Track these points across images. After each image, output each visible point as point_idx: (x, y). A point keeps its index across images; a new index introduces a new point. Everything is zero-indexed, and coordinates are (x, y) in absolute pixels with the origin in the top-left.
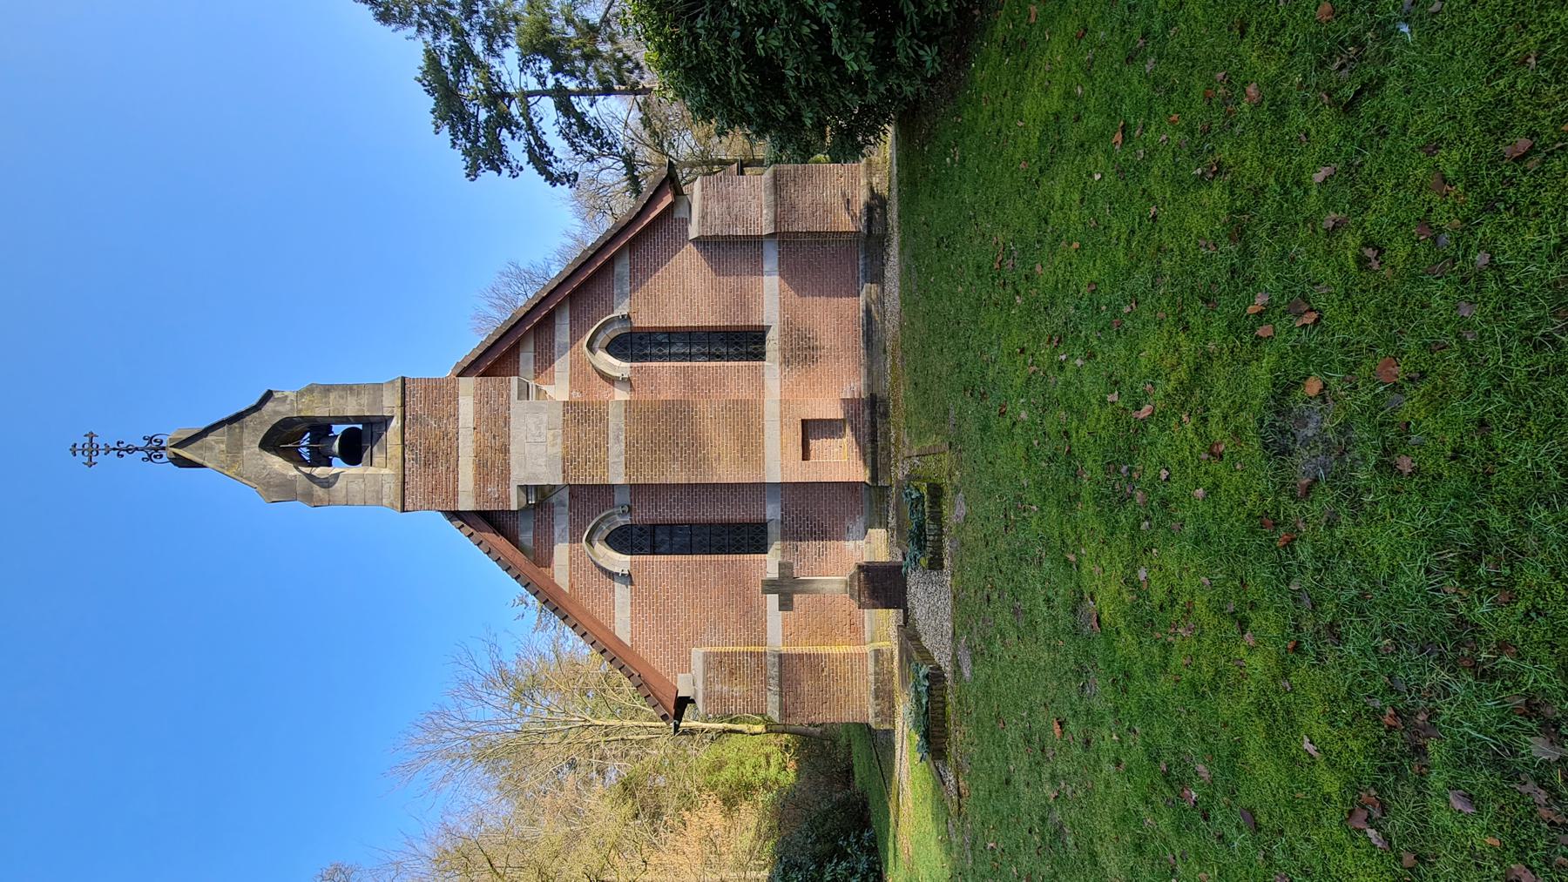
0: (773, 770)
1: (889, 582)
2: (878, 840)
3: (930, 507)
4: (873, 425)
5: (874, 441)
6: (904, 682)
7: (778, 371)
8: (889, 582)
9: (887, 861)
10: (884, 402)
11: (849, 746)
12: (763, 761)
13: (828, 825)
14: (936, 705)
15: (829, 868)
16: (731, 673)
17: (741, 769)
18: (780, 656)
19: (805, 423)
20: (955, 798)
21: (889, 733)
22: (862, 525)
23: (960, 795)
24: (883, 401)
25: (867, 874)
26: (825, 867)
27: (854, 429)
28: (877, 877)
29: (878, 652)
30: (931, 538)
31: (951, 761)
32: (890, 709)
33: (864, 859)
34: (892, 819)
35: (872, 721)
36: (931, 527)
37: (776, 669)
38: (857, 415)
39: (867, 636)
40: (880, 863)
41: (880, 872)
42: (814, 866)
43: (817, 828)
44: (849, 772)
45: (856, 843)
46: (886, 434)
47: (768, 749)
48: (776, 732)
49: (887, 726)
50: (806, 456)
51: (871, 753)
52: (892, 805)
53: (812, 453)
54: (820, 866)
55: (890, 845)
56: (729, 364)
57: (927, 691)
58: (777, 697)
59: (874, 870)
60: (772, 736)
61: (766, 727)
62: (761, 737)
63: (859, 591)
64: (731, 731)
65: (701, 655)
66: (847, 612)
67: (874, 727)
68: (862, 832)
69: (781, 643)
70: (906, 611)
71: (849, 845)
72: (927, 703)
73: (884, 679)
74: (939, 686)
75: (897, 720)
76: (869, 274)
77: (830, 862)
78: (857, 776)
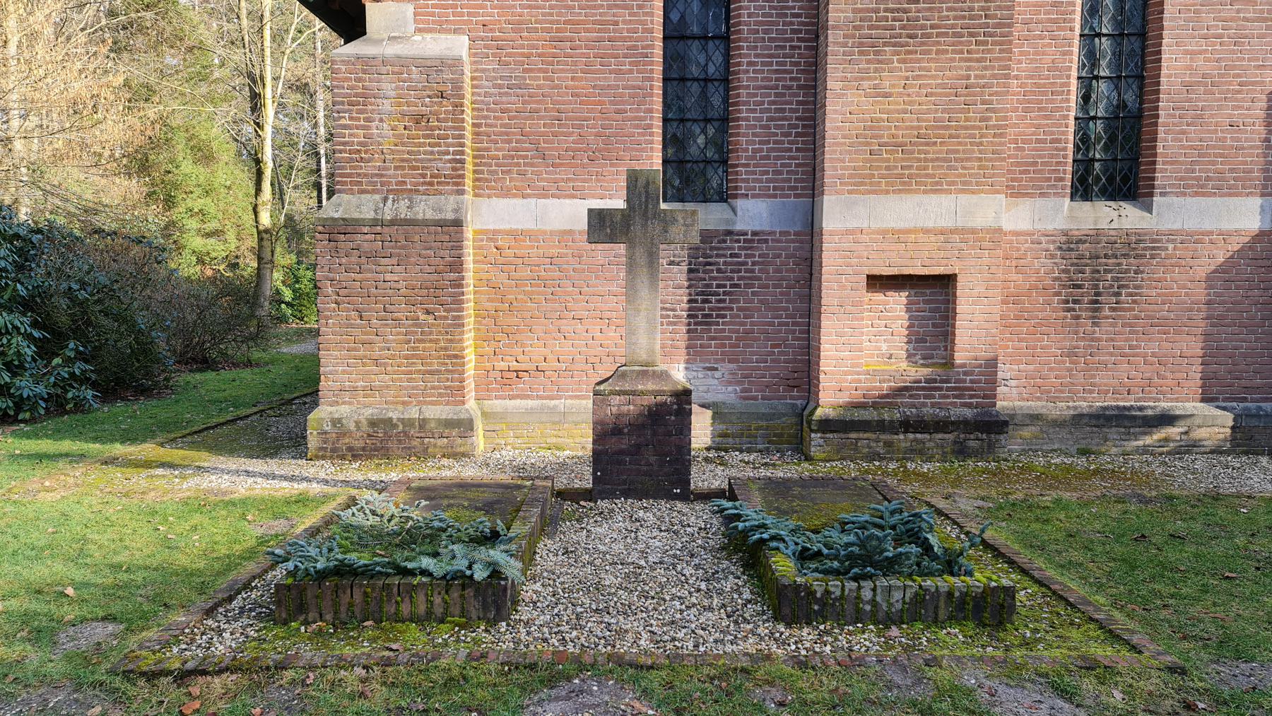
0: (198, 243)
1: (653, 459)
2: (79, 416)
3: (950, 594)
4: (941, 426)
5: (906, 425)
6: (430, 493)
7: (1050, 227)
8: (653, 459)
9: (37, 436)
10: (988, 451)
11: (249, 364)
12: (212, 225)
13: (104, 321)
14: (422, 598)
15: (23, 321)
16: (418, 119)
17: (198, 191)
18: (458, 223)
19: (944, 283)
20: (174, 658)
21: (295, 444)
22: (720, 398)
23: (183, 677)
24: (991, 447)
25: (11, 396)
26: (24, 315)
27: (930, 386)
28: (6, 414)
29: (466, 426)
30: (867, 594)
31: (277, 644)
32: (350, 449)
33: (41, 389)
34: (118, 449)
35: (322, 414)
36: (897, 595)
37: (430, 215)
38: (960, 391)
39: (496, 405)
40: (32, 421)
41: (15, 421)
42: (23, 293)
43: (99, 301)
44: (205, 364)
45: (72, 375)
46: (920, 452)
47: (231, 236)
48: (261, 247)
49: (313, 442)
50: (878, 282)
51: (245, 405)
52: (148, 450)
53: (879, 297)
54: (26, 305)
55: (66, 445)
56: (1072, 122)
57: (458, 575)
58: (371, 215)
59: (19, 406)
60: (252, 242)
61: (267, 231)
62: (248, 218)
63: (634, 393)
64: (259, 174)
65: (455, 53)
66: (542, 365)
67: (311, 417)
68: (94, 386)
69: (479, 227)
70: (589, 495)
71: (68, 361)
72: (425, 572)
73: (410, 438)
74: (474, 609)
75: (327, 463)
76: (1254, 422)
77: (35, 324)
78: (198, 376)
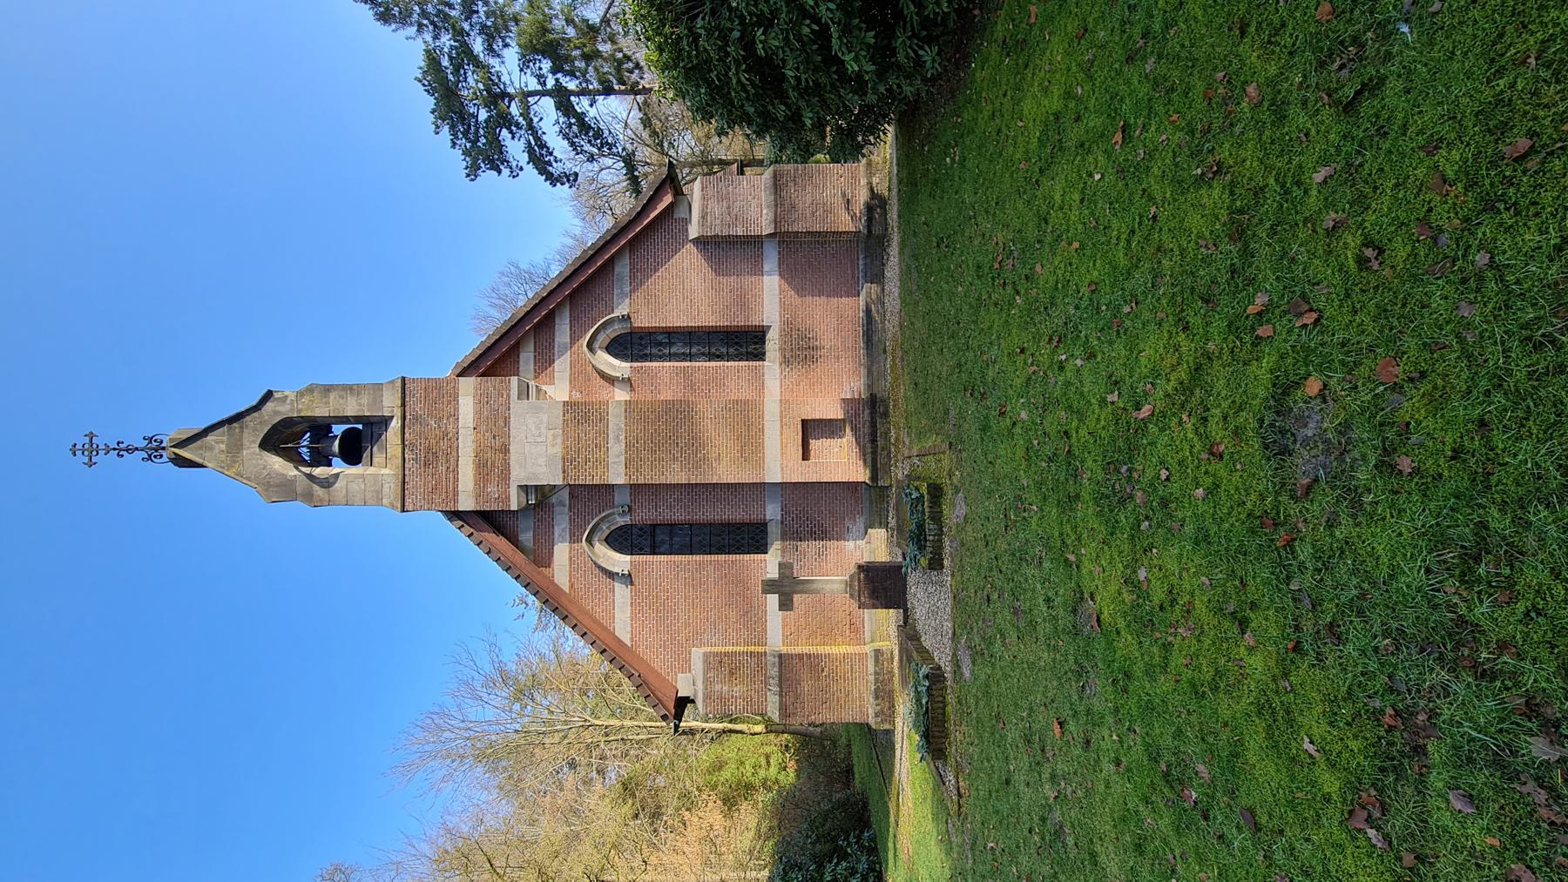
0: (773, 770)
1: (889, 582)
2: (878, 840)
3: (930, 507)
4: (873, 425)
5: (874, 441)
6: (904, 682)
7: (778, 371)
8: (889, 582)
9: (887, 861)
10: (884, 402)
11: (849, 746)
12: (763, 761)
13: (828, 825)
14: (936, 705)
15: (829, 868)
16: (731, 673)
17: (741, 769)
18: (780, 656)
19: (805, 423)
20: (955, 798)
21: (889, 733)
22: (862, 525)
23: (960, 795)
24: (883, 401)
25: (867, 874)
26: (825, 867)
27: (854, 429)
28: (877, 877)
29: (878, 652)
30: (931, 538)
31: (951, 761)
32: (890, 709)
33: (864, 859)
34: (892, 819)
35: (872, 721)
36: (931, 527)
37: (776, 669)
38: (857, 415)
39: (867, 636)
40: (880, 863)
41: (880, 872)
42: (814, 866)
43: (817, 828)
44: (849, 772)
45: (856, 843)
46: (886, 434)
47: (768, 749)
48: (776, 732)
49: (887, 726)
50: (806, 456)
51: (871, 753)
52: (892, 805)
53: (812, 453)
54: (820, 866)
55: (890, 845)
56: (729, 364)
57: (927, 691)
58: (777, 697)
59: (874, 870)
60: (772, 736)
61: (766, 727)
62: (761, 737)
63: (859, 591)
64: (731, 731)
65: (701, 655)
66: (847, 612)
67: (874, 727)
68: (862, 832)
69: (781, 643)
70: (906, 611)
71: (849, 845)
72: (927, 703)
73: (884, 679)
74: (939, 686)
75: (897, 720)
76: (869, 274)
77: (830, 862)
78: (857, 776)
